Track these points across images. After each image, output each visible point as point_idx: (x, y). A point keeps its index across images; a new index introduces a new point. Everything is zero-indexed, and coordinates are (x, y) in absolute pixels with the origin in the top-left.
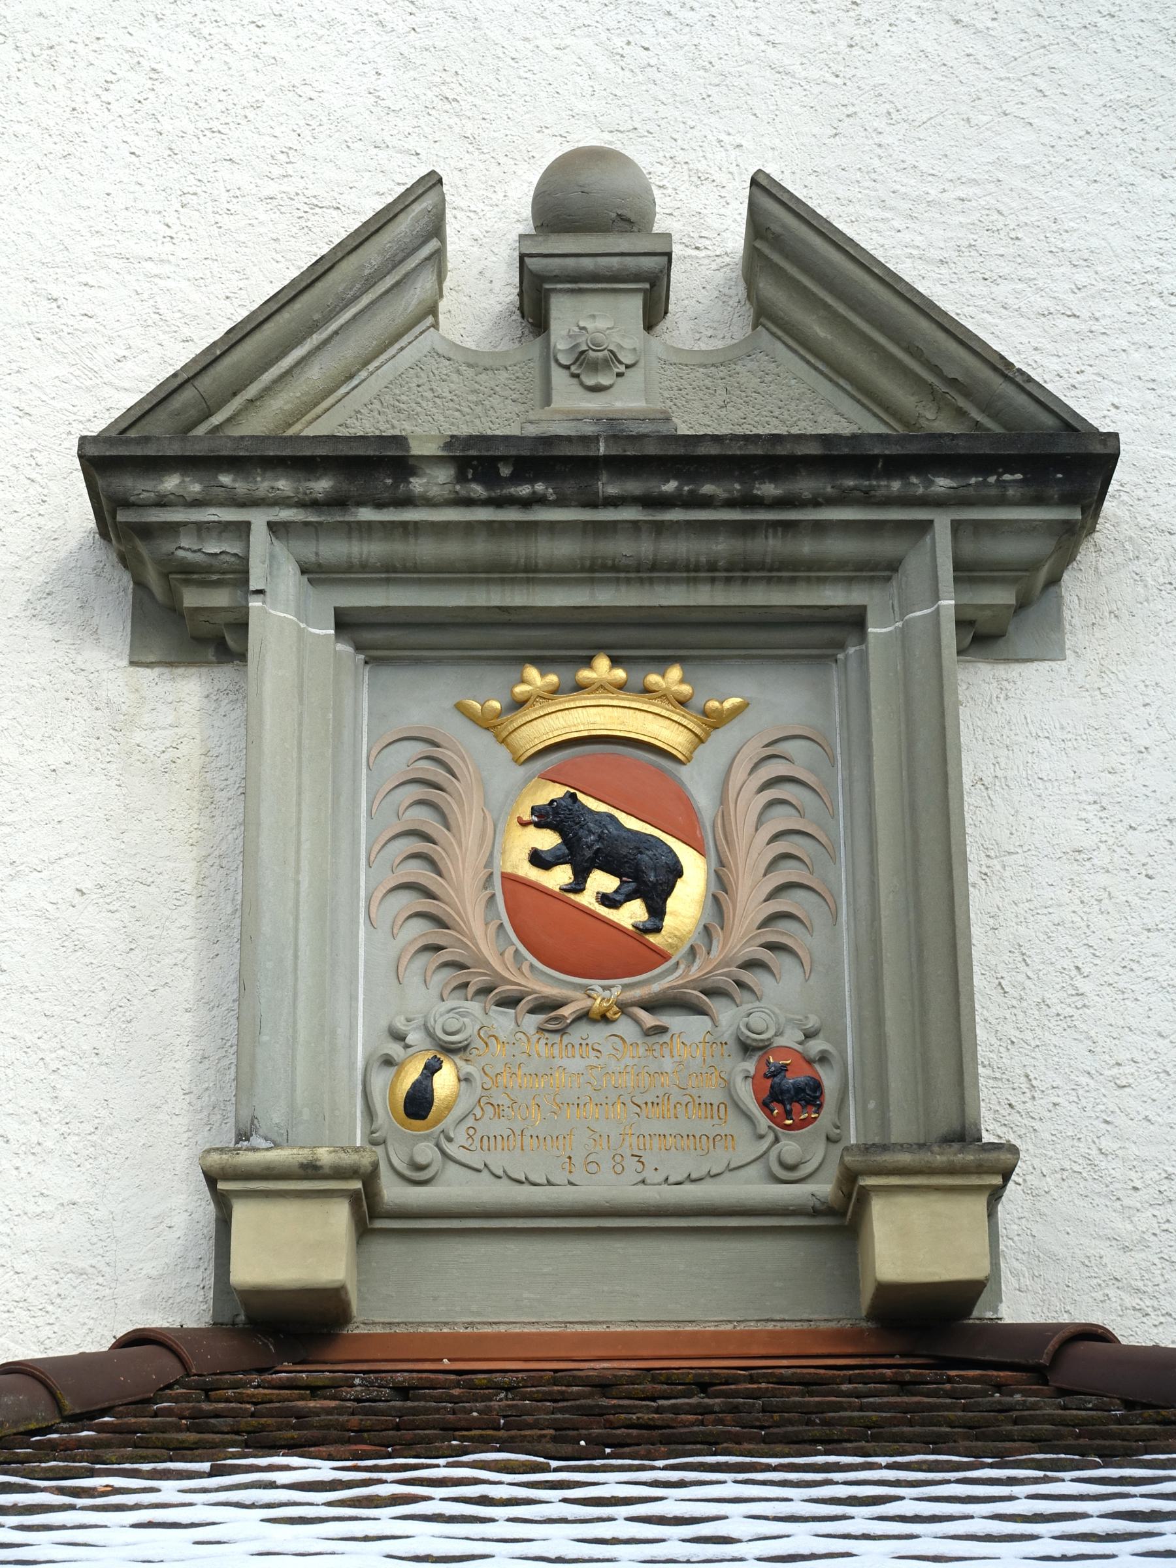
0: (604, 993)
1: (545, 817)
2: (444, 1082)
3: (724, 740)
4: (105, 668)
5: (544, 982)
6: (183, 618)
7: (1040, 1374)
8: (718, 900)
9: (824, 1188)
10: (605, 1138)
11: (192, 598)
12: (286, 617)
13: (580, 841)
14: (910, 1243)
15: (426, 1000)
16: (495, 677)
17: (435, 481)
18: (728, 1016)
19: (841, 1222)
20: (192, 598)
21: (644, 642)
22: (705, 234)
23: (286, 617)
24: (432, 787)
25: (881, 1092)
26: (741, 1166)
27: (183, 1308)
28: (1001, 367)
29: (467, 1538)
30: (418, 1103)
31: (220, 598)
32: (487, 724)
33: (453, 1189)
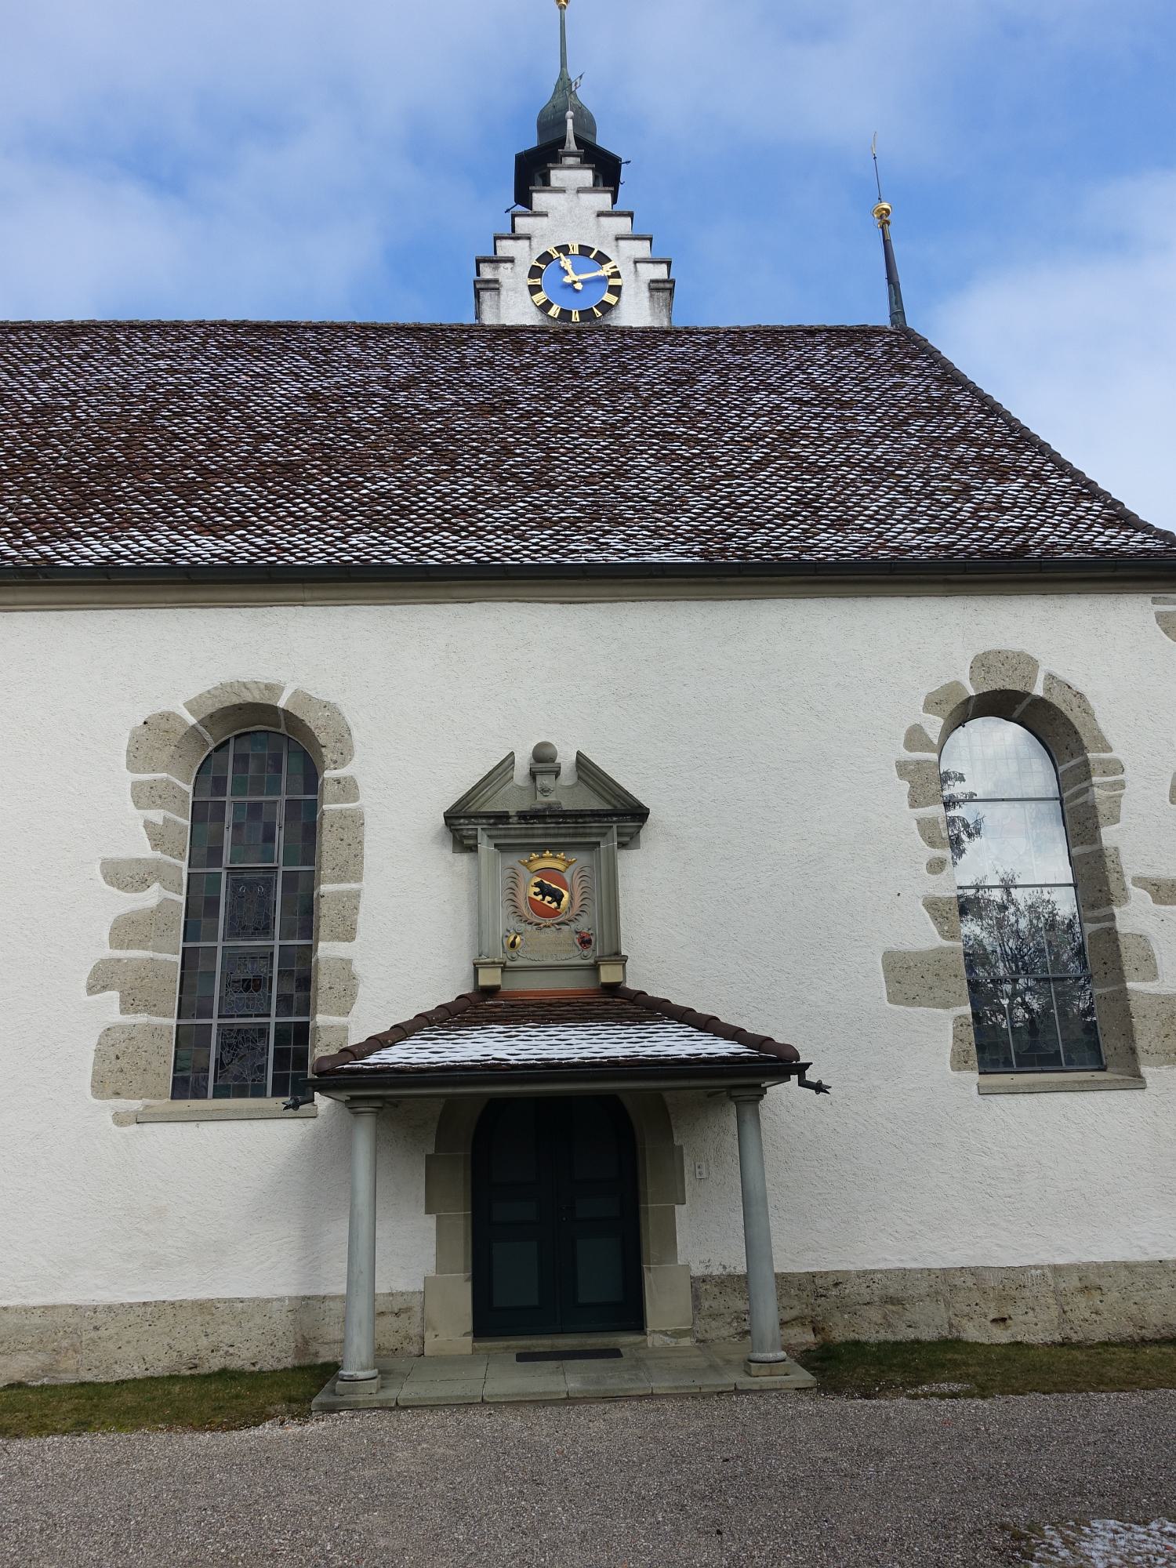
0: (549, 921)
1: (537, 885)
2: (518, 940)
3: (572, 867)
4: (447, 852)
5: (537, 919)
7: (632, 1001)
8: (571, 897)
9: (592, 961)
10: (549, 957)
11: (466, 842)
12: (485, 846)
13: (544, 890)
14: (608, 974)
15: (513, 923)
16: (526, 855)
17: (514, 820)
18: (573, 926)
19: (595, 968)
20: (466, 842)
21: (555, 848)
22: (566, 759)
23: (485, 846)
24: (514, 878)
27: (467, 990)
28: (627, 793)
30: (513, 945)
31: (471, 842)
32: (524, 864)
33: (519, 963)
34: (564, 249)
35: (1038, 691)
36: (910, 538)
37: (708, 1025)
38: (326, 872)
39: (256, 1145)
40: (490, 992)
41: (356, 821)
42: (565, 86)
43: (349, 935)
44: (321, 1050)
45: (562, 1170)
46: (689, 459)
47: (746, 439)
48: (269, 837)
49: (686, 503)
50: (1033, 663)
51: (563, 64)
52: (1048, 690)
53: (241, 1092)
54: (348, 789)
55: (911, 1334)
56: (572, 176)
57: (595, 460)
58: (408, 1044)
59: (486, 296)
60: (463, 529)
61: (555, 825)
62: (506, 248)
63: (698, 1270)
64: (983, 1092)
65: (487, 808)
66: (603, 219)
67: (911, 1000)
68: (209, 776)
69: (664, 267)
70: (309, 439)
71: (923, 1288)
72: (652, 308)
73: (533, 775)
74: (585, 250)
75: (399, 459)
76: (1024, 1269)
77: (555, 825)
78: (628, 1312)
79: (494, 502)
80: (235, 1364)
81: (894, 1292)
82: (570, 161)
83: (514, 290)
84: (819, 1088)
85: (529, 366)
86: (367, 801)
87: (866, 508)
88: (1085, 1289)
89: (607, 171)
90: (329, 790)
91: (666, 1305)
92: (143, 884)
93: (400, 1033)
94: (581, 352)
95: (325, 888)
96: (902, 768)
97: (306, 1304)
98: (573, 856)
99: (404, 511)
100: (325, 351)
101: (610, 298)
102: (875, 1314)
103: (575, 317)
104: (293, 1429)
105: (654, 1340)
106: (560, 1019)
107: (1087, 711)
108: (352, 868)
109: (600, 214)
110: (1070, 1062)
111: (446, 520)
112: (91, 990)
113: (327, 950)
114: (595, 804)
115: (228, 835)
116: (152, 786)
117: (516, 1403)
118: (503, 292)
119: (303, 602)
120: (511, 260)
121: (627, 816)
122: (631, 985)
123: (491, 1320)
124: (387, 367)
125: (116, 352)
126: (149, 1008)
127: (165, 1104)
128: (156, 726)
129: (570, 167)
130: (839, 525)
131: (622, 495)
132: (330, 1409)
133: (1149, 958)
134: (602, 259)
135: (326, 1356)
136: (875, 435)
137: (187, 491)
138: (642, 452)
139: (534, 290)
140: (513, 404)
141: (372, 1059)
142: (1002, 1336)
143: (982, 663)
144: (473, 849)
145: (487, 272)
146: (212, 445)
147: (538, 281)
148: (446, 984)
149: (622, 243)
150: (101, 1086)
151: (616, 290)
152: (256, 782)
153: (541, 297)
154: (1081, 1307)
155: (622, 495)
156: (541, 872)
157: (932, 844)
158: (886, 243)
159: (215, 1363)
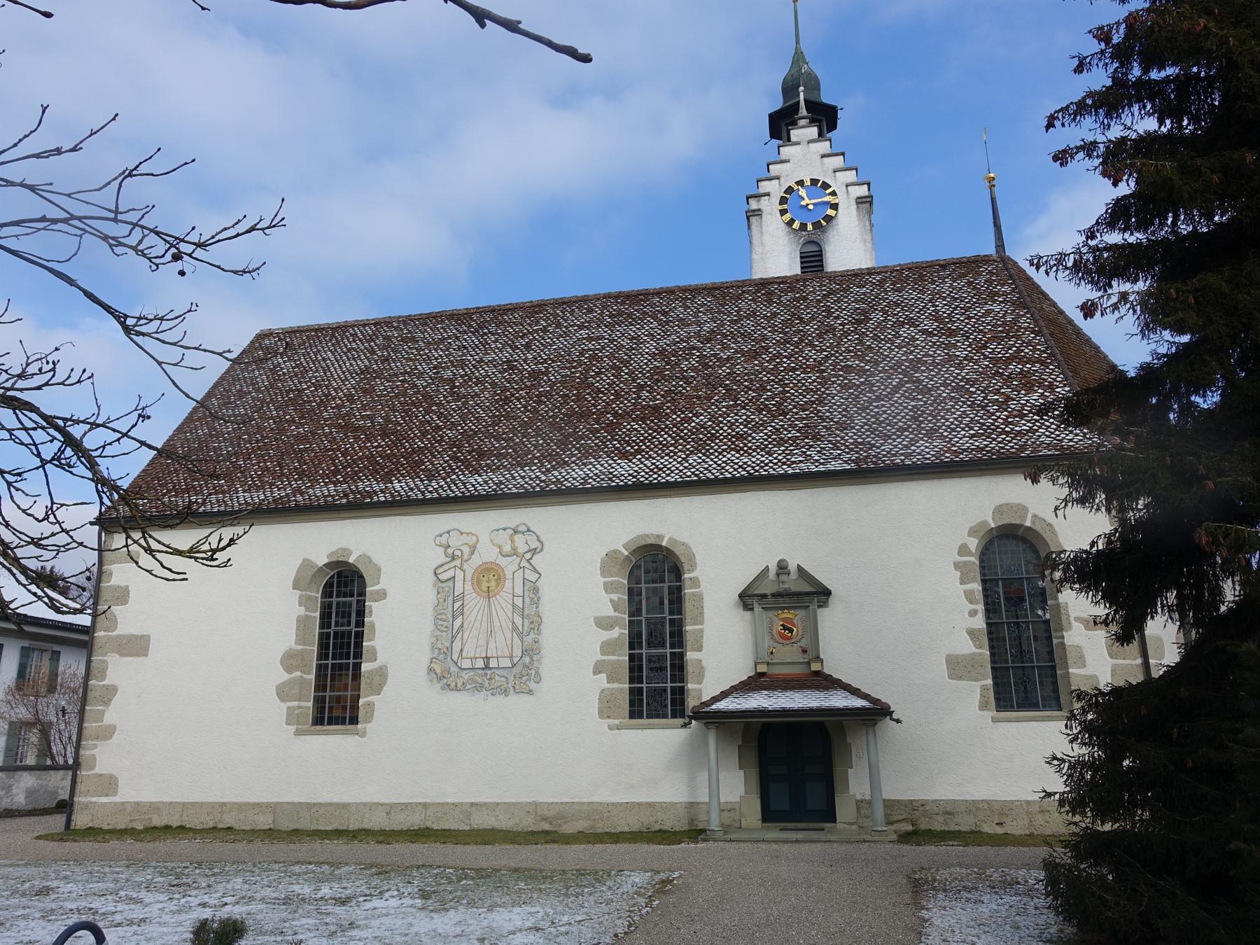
4: (741, 611)
6: (747, 607)
10: (788, 659)
12: (757, 609)
13: (785, 628)
14: (815, 667)
19: (809, 663)
22: (792, 567)
23: (757, 609)
24: (771, 623)
25: (812, 653)
26: (801, 658)
29: (219, 267)
34: (801, 183)
35: (1028, 523)
36: (966, 443)
37: (855, 692)
38: (688, 621)
39: (664, 740)
40: (762, 674)
41: (700, 597)
42: (798, 58)
43: (700, 649)
44: (691, 703)
45: (799, 756)
46: (858, 386)
47: (891, 368)
48: (662, 603)
49: (853, 421)
50: (1025, 509)
51: (797, 42)
52: (1033, 523)
53: (658, 717)
54: (695, 582)
55: (957, 828)
56: (804, 132)
57: (808, 390)
58: (727, 700)
59: (753, 219)
60: (742, 449)
61: (790, 598)
62: (765, 186)
63: (859, 797)
64: (994, 720)
65: (757, 592)
66: (825, 159)
67: (960, 678)
68: (633, 575)
69: (866, 187)
70: (664, 387)
71: (963, 808)
72: (859, 216)
73: (778, 575)
74: (814, 182)
75: (709, 398)
76: (1013, 802)
77: (790, 598)
78: (829, 814)
79: (756, 428)
80: (665, 828)
81: (950, 810)
82: (802, 122)
83: (771, 214)
84: (898, 721)
85: (775, 315)
86: (704, 588)
87: (947, 420)
88: (1042, 811)
89: (825, 117)
90: (687, 583)
91: (845, 811)
92: (611, 627)
93: (724, 695)
94: (805, 299)
95: (688, 628)
96: (957, 566)
97: (691, 805)
98: (798, 612)
99: (713, 438)
100: (665, 313)
101: (831, 212)
102: (940, 819)
103: (810, 227)
104: (692, 845)
105: (839, 826)
106: (792, 688)
107: (1054, 533)
108: (699, 619)
109: (823, 156)
110: (1044, 706)
111: (733, 443)
112: (595, 673)
113: (690, 656)
114: (808, 589)
115: (644, 602)
116: (612, 583)
117: (776, 842)
118: (764, 216)
119: (670, 496)
120: (768, 194)
121: (822, 594)
122: (826, 671)
123: (769, 815)
124: (699, 324)
125: (559, 325)
126: (618, 681)
127: (627, 721)
128: (611, 556)
129: (803, 127)
130: (930, 434)
131: (821, 417)
132: (706, 840)
133: (1082, 657)
134: (826, 186)
135: (701, 826)
136: (965, 359)
137: (611, 428)
138: (834, 382)
139: (783, 212)
140: (767, 348)
141: (714, 707)
142: (1000, 830)
143: (999, 510)
144: (752, 609)
145: (754, 205)
146: (617, 395)
147: (785, 206)
148: (742, 672)
149: (838, 174)
150: (601, 714)
151: (835, 207)
152: (655, 583)
153: (788, 217)
154: (1040, 820)
155: (821, 417)
156: (784, 619)
157: (971, 602)
158: (993, 200)
159: (657, 827)
